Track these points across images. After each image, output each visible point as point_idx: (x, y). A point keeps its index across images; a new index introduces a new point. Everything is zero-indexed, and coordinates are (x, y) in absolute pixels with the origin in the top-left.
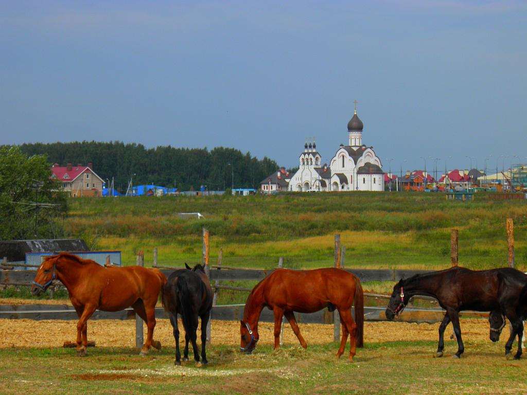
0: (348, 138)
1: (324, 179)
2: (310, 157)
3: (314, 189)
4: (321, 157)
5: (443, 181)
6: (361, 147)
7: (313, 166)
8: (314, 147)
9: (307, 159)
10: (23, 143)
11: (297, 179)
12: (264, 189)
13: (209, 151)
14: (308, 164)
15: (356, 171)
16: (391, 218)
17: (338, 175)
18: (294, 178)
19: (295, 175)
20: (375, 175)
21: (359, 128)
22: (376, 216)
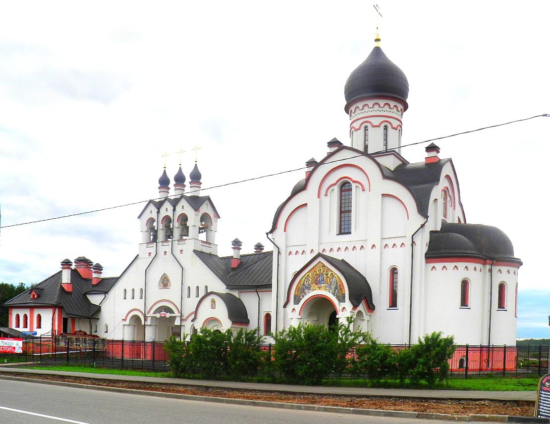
1: (236, 293)
9: (167, 220)
12: (18, 326)
14: (169, 234)
15: (422, 246)
16: (483, 402)
22: (486, 403)
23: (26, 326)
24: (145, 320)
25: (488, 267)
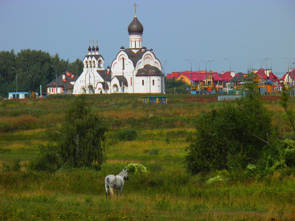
0: (128, 41)
2: (93, 60)
3: (97, 92)
4: (104, 59)
5: (205, 81)
6: (140, 49)
7: (97, 68)
8: (97, 49)
10: (21, 50)
11: (82, 81)
12: (50, 92)
13: (16, 54)
15: (135, 73)
17: (118, 77)
18: (78, 81)
19: (79, 78)
20: (154, 77)
21: (139, 31)
23: (53, 92)
24: (86, 88)
25: (149, 77)
